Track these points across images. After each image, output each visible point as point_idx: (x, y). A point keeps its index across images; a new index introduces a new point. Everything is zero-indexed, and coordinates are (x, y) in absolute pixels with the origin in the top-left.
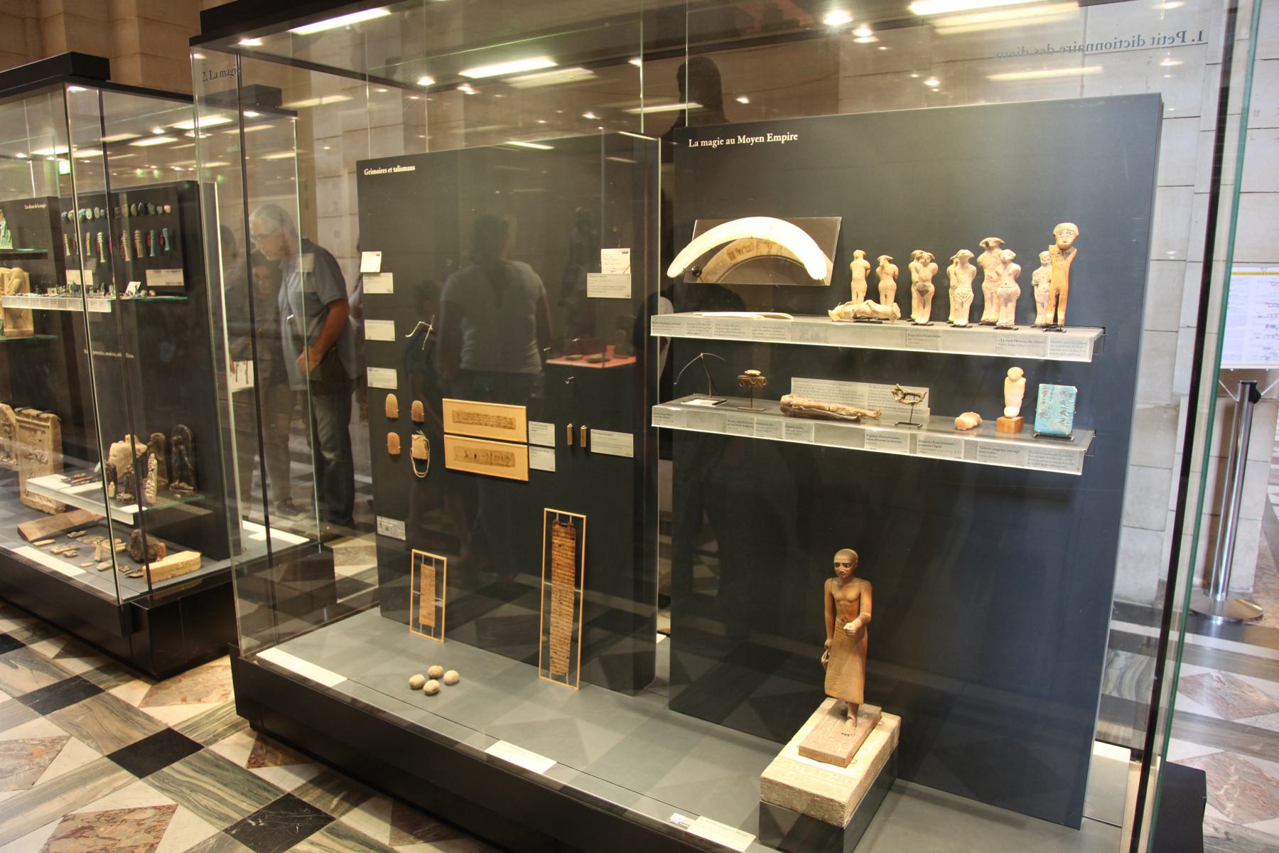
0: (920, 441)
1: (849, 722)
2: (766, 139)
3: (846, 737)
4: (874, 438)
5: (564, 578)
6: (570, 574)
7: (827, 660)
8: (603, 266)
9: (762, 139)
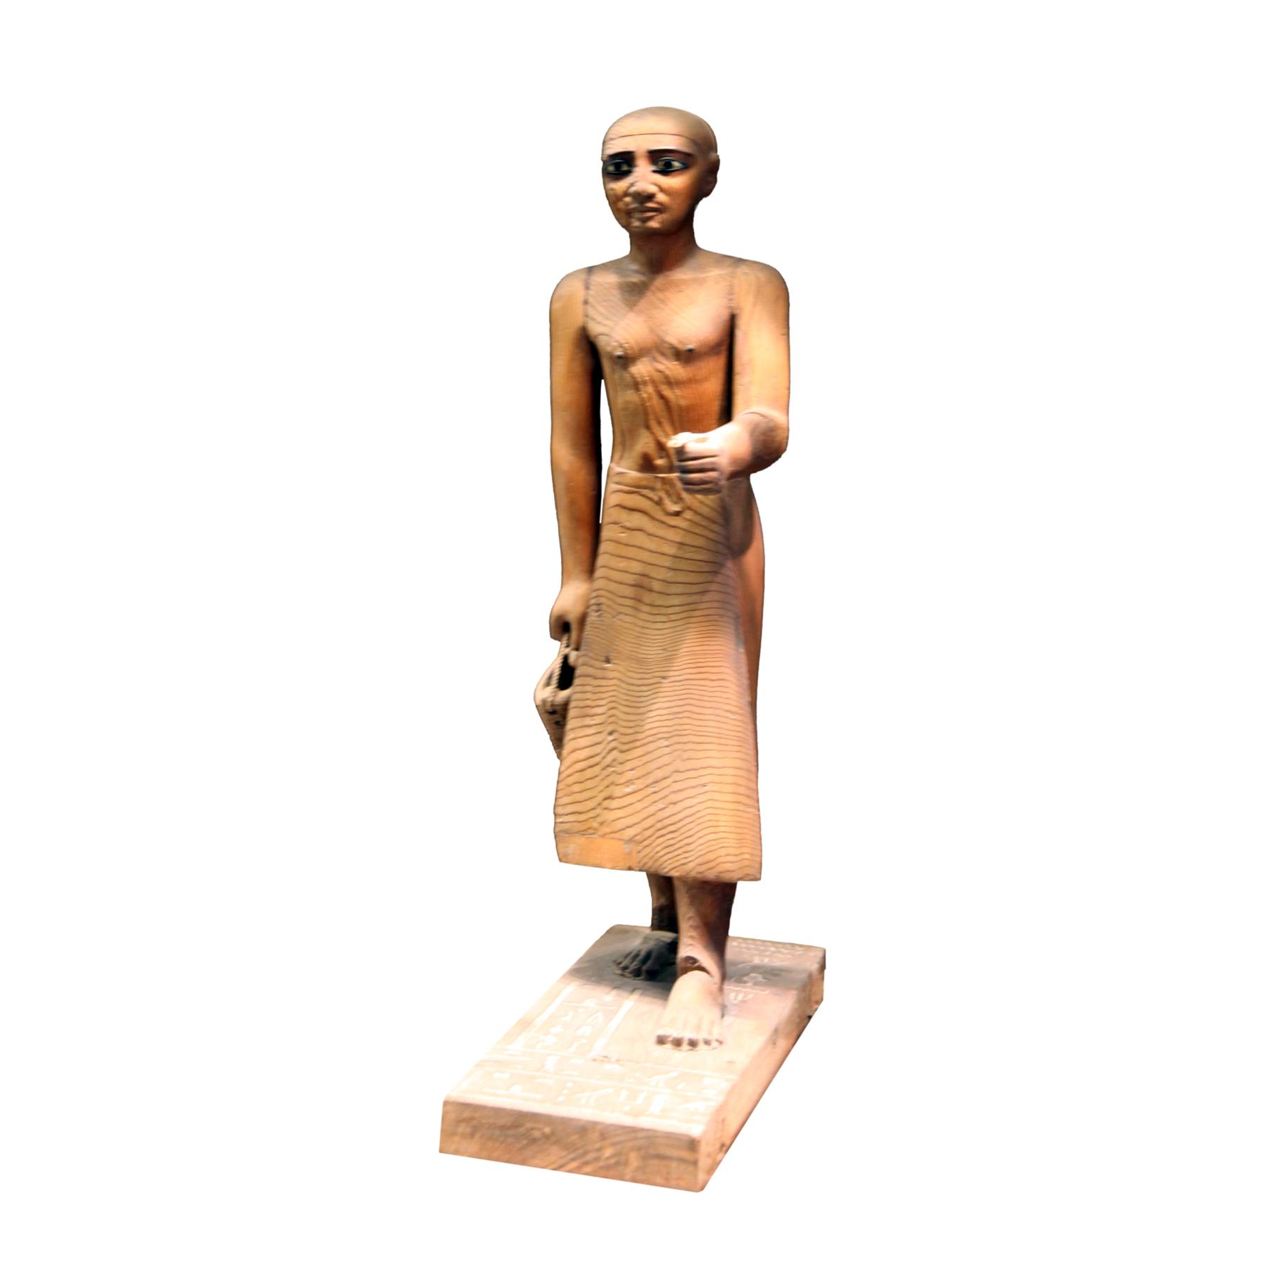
1: (688, 986)
3: (684, 1053)
7: (564, 694)
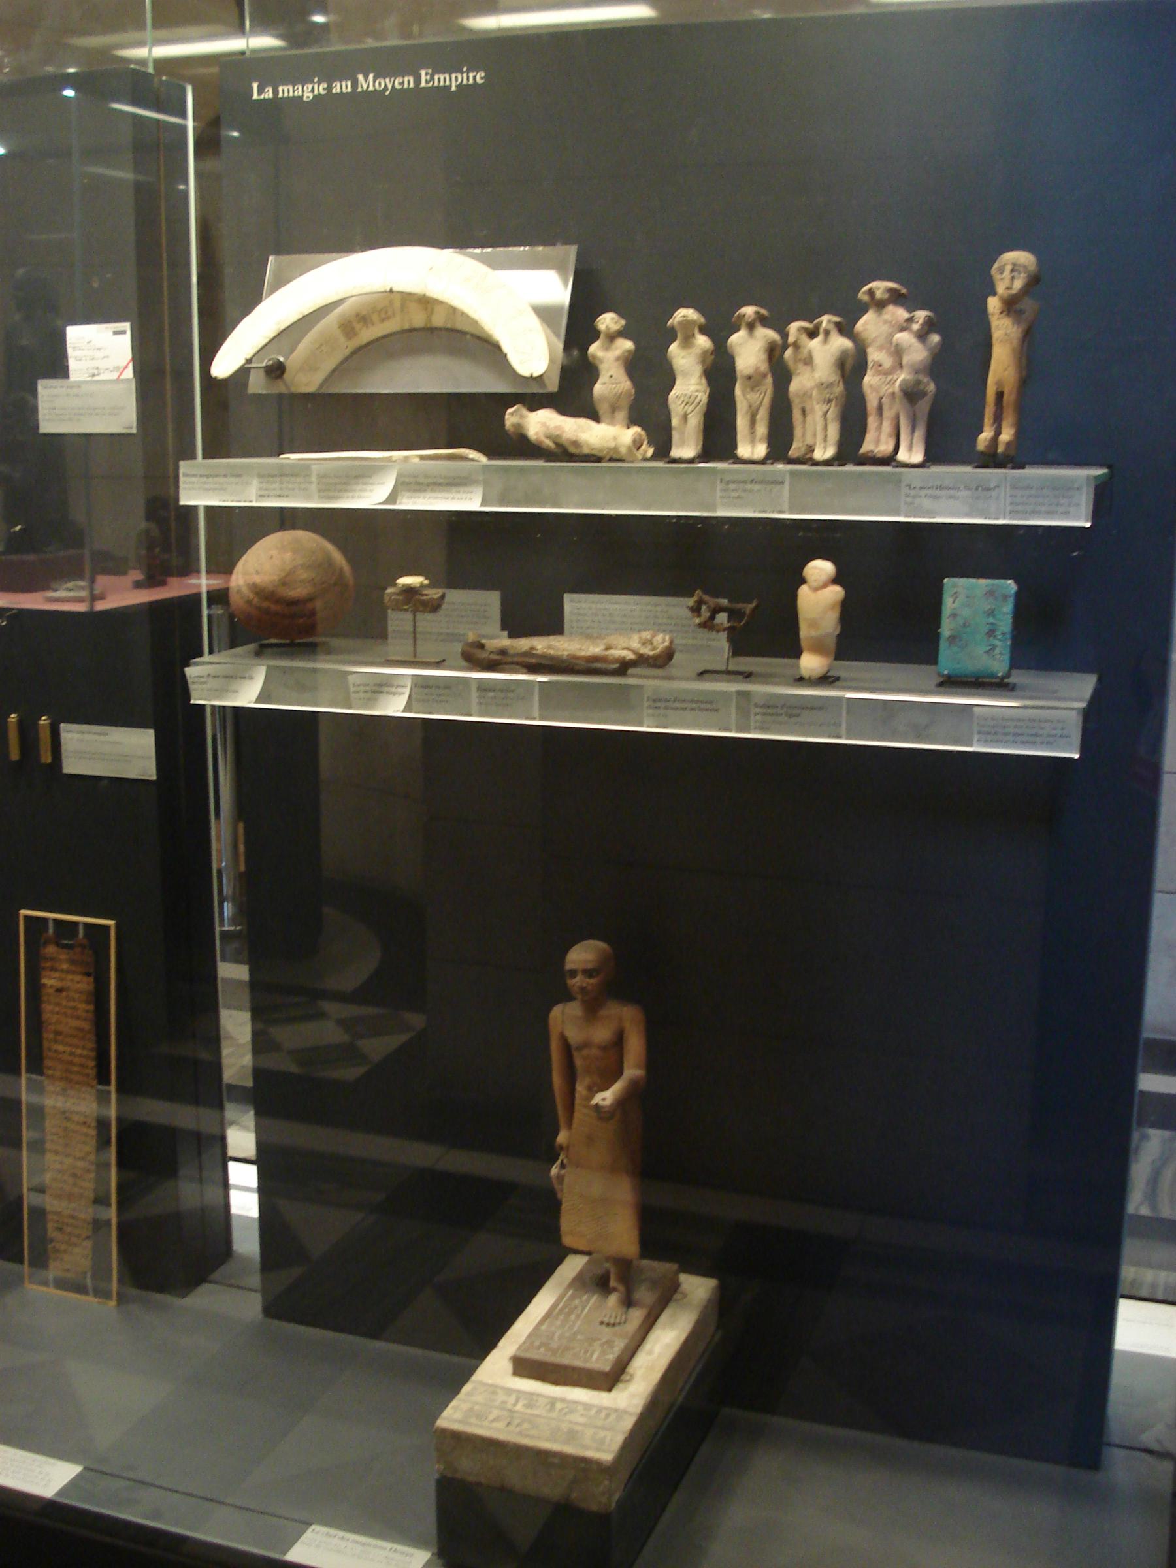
0: (756, 705)
1: (613, 1299)
2: (418, 80)
4: (663, 705)
5: (71, 1063)
6: (85, 1053)
7: (563, 1172)
8: (72, 364)
9: (408, 82)
